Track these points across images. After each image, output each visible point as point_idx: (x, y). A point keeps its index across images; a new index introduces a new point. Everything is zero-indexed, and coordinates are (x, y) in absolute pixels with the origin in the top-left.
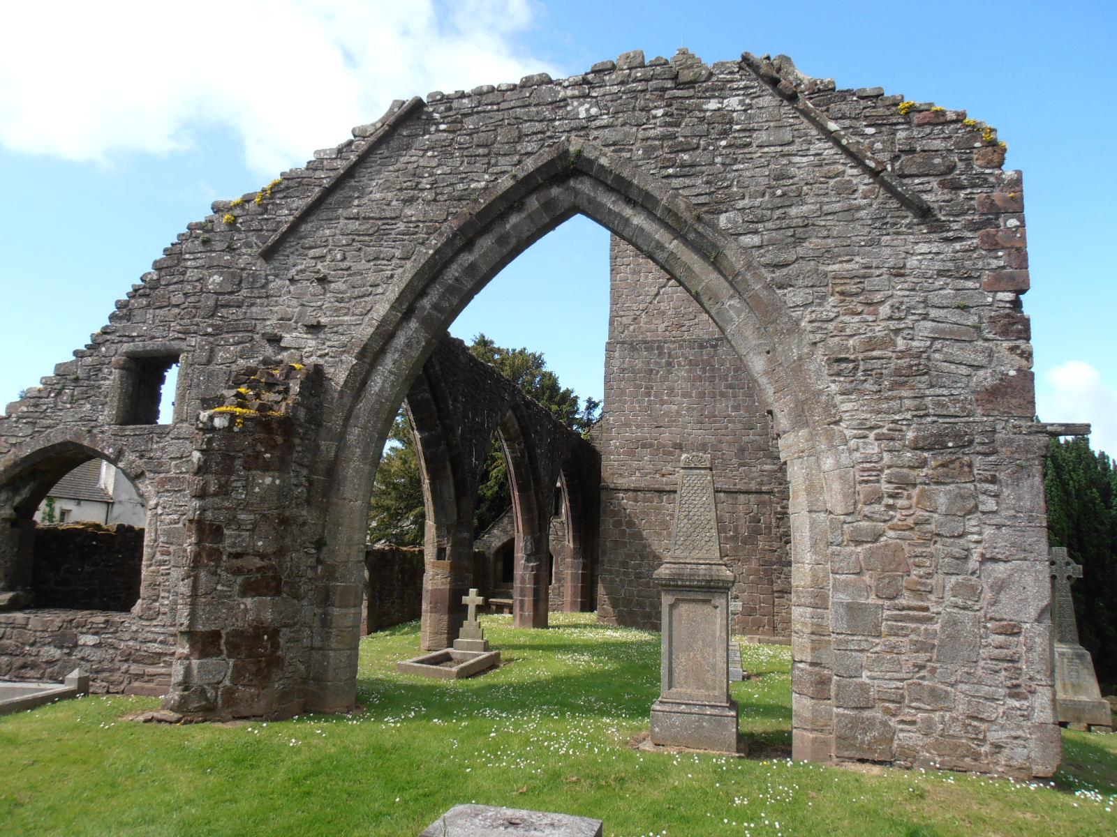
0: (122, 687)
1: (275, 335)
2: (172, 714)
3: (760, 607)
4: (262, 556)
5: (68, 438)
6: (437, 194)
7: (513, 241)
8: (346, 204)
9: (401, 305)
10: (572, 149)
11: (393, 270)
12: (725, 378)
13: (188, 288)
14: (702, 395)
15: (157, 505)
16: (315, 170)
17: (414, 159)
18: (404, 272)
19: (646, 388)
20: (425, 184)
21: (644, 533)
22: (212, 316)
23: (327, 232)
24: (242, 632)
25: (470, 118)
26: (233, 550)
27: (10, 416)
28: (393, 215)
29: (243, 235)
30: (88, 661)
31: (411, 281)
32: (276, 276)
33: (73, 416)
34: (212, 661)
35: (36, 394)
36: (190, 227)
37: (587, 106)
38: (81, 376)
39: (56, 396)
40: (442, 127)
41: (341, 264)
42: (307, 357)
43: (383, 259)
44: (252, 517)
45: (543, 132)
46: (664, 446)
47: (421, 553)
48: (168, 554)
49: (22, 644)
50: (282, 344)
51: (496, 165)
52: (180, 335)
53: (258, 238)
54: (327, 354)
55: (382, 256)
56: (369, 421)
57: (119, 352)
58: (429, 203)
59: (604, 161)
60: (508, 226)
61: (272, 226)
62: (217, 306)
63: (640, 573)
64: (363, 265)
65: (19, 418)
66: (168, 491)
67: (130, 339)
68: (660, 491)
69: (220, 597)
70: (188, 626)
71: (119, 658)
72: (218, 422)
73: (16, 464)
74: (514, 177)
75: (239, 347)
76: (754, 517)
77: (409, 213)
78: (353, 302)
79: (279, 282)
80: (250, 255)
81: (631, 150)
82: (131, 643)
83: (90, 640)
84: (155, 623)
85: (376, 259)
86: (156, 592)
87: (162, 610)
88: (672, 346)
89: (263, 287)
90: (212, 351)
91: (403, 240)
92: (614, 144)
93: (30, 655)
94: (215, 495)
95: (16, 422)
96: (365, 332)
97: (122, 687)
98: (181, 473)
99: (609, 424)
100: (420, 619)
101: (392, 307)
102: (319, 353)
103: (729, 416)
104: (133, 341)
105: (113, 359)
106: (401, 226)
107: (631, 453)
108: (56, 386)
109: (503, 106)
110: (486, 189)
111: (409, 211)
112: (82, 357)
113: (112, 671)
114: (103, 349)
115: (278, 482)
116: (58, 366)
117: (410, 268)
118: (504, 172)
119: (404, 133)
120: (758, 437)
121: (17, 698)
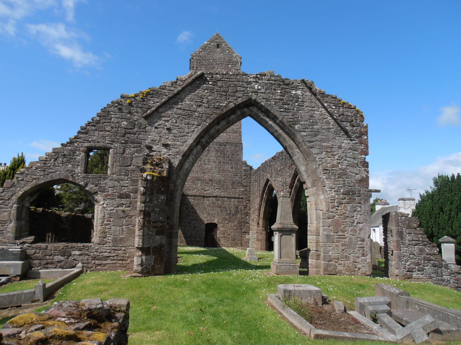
0: (92, 269)
2: (139, 274)
3: (238, 238)
4: (162, 222)
5: (62, 177)
8: (177, 104)
11: (194, 128)
13: (113, 125)
14: (220, 162)
15: (103, 204)
16: (163, 89)
17: (200, 92)
18: (198, 130)
20: (205, 101)
23: (170, 112)
28: (194, 110)
29: (135, 108)
32: (149, 125)
33: (64, 169)
34: (149, 257)
35: (45, 159)
38: (66, 154)
39: (54, 161)
40: (210, 83)
41: (175, 124)
42: (163, 155)
43: (191, 124)
44: (158, 209)
48: (110, 221)
49: (45, 255)
50: (153, 149)
51: (229, 99)
54: (171, 154)
55: (190, 123)
58: (206, 108)
59: (263, 104)
60: (230, 119)
62: (125, 133)
63: (196, 226)
66: (109, 199)
68: (204, 197)
69: (150, 236)
72: (149, 178)
73: (36, 186)
74: (235, 104)
75: (135, 149)
77: (200, 110)
78: (180, 138)
79: (150, 127)
82: (95, 253)
83: (77, 253)
84: (105, 245)
85: (188, 124)
86: (105, 235)
87: (108, 241)
89: (144, 128)
90: (124, 149)
92: (266, 99)
93: (50, 259)
94: (148, 202)
95: (35, 170)
98: (114, 193)
100: (266, 250)
101: (194, 141)
102: (168, 154)
104: (90, 143)
105: (81, 149)
106: (197, 114)
107: (193, 182)
108: (54, 157)
110: (225, 106)
111: (199, 109)
112: (66, 146)
113: (88, 263)
116: (54, 149)
117: (200, 129)
118: (232, 102)
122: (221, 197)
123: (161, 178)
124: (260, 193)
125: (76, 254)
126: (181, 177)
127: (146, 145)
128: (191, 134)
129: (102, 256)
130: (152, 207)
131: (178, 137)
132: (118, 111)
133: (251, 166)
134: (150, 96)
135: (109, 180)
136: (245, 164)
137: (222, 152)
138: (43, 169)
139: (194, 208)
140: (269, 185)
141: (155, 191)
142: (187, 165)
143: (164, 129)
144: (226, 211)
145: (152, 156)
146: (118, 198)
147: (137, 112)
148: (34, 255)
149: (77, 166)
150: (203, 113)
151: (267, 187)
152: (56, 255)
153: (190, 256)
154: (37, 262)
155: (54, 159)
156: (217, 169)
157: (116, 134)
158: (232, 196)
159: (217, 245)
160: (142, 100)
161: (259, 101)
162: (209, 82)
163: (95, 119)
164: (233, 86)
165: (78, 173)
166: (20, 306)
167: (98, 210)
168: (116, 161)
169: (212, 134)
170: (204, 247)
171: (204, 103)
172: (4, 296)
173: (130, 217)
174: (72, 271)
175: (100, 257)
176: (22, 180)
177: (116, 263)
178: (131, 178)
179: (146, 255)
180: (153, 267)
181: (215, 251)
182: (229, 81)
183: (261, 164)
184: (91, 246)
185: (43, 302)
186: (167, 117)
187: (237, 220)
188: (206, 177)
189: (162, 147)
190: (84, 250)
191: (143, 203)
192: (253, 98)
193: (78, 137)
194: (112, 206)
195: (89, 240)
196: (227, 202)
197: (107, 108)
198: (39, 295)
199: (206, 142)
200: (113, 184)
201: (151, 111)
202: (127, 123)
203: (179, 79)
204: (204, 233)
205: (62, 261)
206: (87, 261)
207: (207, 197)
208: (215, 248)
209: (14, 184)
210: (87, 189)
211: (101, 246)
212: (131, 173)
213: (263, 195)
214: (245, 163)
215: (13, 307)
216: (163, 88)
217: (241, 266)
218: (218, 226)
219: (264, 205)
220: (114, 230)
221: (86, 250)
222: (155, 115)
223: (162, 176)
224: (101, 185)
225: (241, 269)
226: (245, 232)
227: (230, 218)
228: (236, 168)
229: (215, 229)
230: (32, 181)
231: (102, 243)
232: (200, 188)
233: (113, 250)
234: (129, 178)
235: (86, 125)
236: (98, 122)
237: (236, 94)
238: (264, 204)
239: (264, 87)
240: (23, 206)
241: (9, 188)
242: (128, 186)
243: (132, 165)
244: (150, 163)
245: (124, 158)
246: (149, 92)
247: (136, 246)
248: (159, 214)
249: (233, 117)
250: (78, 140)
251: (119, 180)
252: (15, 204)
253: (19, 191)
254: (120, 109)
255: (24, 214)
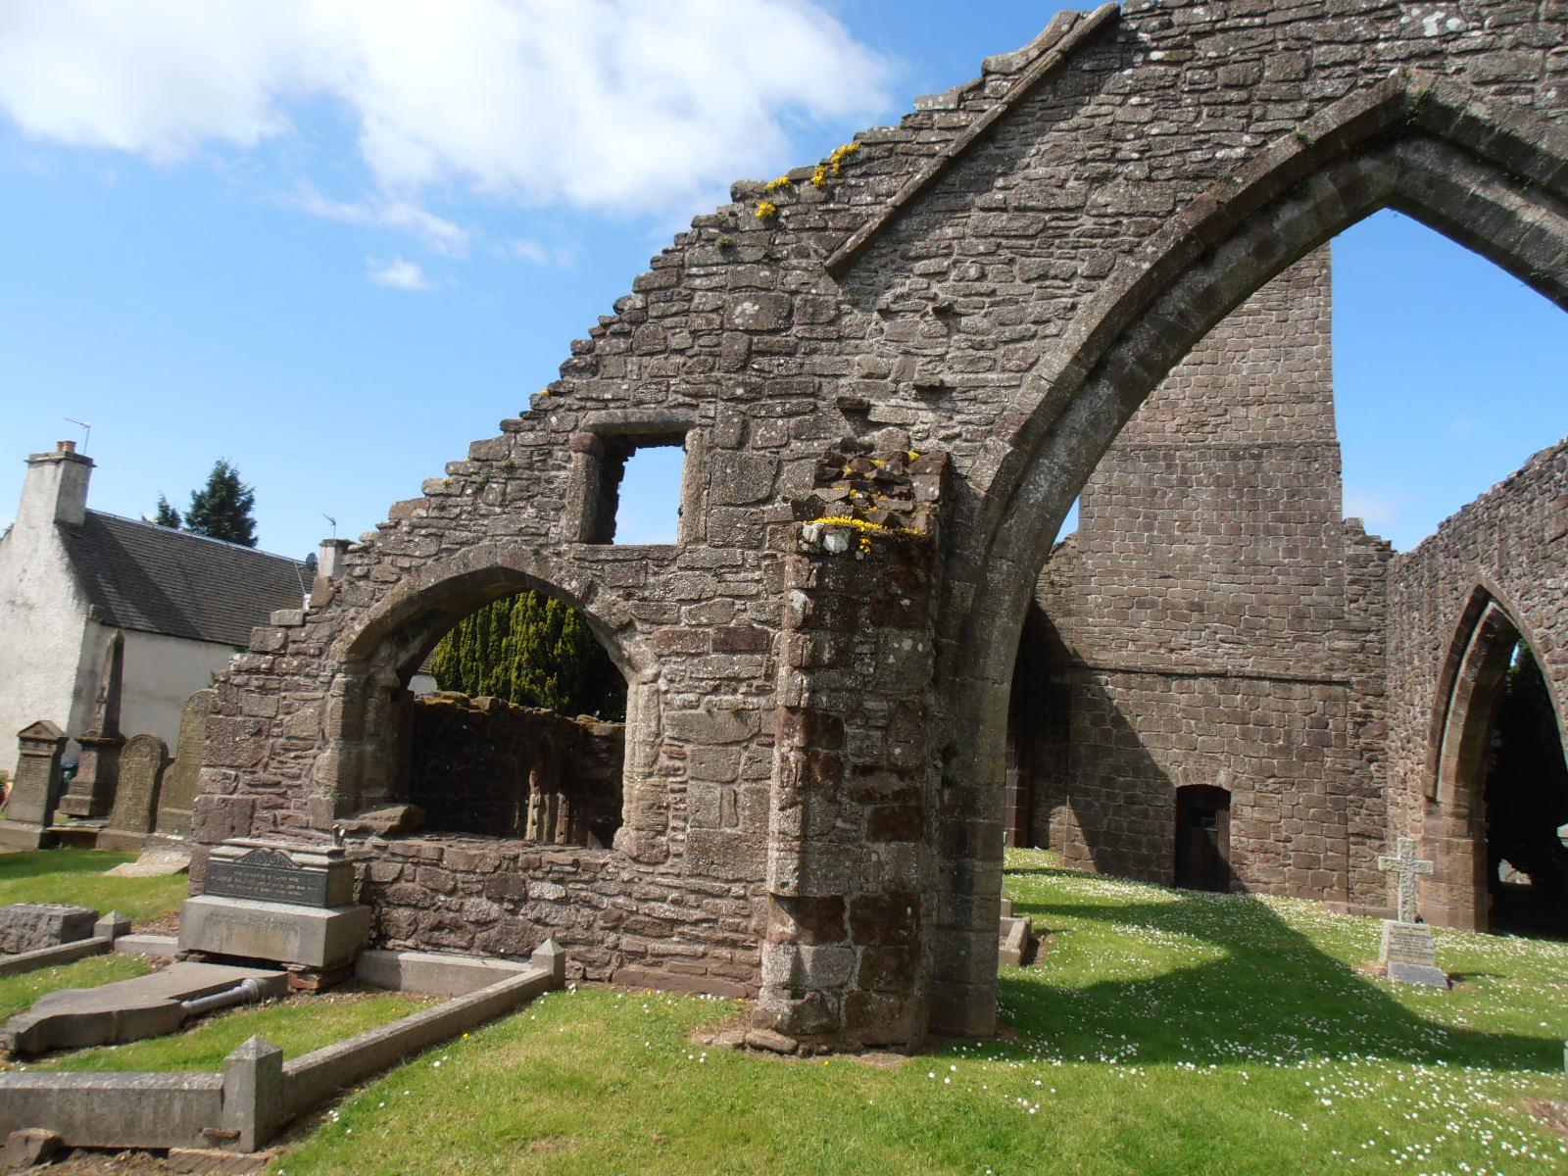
0: (608, 971)
1: (860, 402)
2: (779, 1037)
3: (1327, 858)
4: (902, 773)
5: (499, 560)
6: (1152, 169)
7: (1281, 251)
8: (984, 184)
9: (1087, 357)
10: (1413, 90)
11: (1074, 295)
12: (1272, 505)
13: (699, 322)
14: (1236, 530)
15: (657, 676)
16: (919, 129)
17: (1104, 109)
18: (1096, 300)
19: (1146, 516)
20: (1128, 150)
21: (1141, 737)
22: (743, 368)
23: (949, 232)
24: (876, 900)
25: (1210, 40)
26: (860, 761)
27: (398, 523)
28: (1071, 204)
29: (791, 237)
30: (546, 925)
31: (1109, 316)
32: (855, 304)
33: (506, 527)
34: (833, 948)
35: (441, 489)
36: (696, 224)
37: (1439, 15)
38: (516, 462)
39: (475, 493)
40: (1156, 55)
41: (977, 284)
42: (921, 440)
43: (1055, 277)
44: (884, 705)
45: (1353, 62)
46: (1174, 607)
47: (616, 742)
48: (682, 757)
49: (432, 890)
50: (872, 418)
51: (1262, 118)
52: (688, 400)
53: (819, 241)
54: (959, 435)
55: (1052, 272)
56: (1025, 550)
57: (581, 424)
58: (1137, 182)
59: (1478, 110)
60: (1277, 226)
61: (843, 221)
62: (750, 353)
63: (1134, 796)
64: (1018, 287)
65: (413, 527)
66: (678, 654)
67: (600, 405)
68: (1168, 675)
69: (842, 841)
70: (796, 889)
71: (601, 923)
72: (831, 542)
73: (410, 600)
74: (1301, 139)
75: (793, 421)
76: (1318, 719)
77: (1101, 200)
78: (1001, 350)
79: (858, 316)
80: (805, 269)
81: (1532, 91)
82: (621, 900)
83: (550, 891)
84: (662, 869)
85: (1043, 277)
86: (662, 819)
87: (673, 848)
88: (1188, 455)
89: (832, 322)
90: (745, 426)
91: (1093, 246)
92: (1497, 80)
93: (448, 909)
94: (831, 666)
95: (409, 533)
96: (1028, 398)
97: (608, 971)
98: (699, 625)
99: (1086, 570)
100: (1478, 929)
101: (1076, 359)
102: (943, 433)
103: (1278, 564)
104: (606, 407)
105: (571, 436)
106: (1087, 223)
107: (1121, 615)
108: (474, 478)
109: (1270, 19)
110: (1245, 159)
111: (1099, 197)
112: (517, 432)
113: (590, 943)
114: (554, 419)
115: (920, 647)
116: (476, 446)
117: (1106, 295)
118: (1279, 132)
119: (1086, 67)
120: (1326, 599)
121: (491, 990)
122: (1244, 677)
123: (898, 547)
124: (1436, 659)
125: (547, 896)
126: (1014, 550)
127: (841, 400)
128: (1060, 322)
129: (649, 915)
130: (850, 690)
131: (991, 346)
132: (719, 258)
133: (1384, 539)
134: (858, 172)
135: (680, 569)
136: (1357, 533)
137: (1247, 487)
138: (433, 530)
139: (1124, 719)
140: (1489, 617)
141: (864, 611)
142: (1040, 487)
143: (922, 317)
144: (1269, 737)
145: (871, 448)
146: (715, 650)
147: (802, 253)
148: (397, 886)
149: (557, 510)
150: (1122, 214)
151: (1477, 630)
152: (471, 894)
153: (1097, 930)
154: (402, 914)
155: (474, 486)
156: (1224, 558)
157: (710, 359)
158: (1296, 671)
159: (1233, 883)
160: (823, 195)
161: (1452, 100)
162: (1148, 50)
163: (629, 303)
164: (1286, 49)
165: (558, 543)
166: (162, 1153)
167: (636, 706)
168: (709, 483)
169: (1171, 319)
170: (1173, 884)
171: (1124, 161)
172: (105, 1090)
173: (766, 740)
174: (515, 973)
175: (641, 918)
176: (366, 577)
177: (704, 955)
178: (774, 556)
179: (820, 938)
180: (858, 1002)
181: (1219, 911)
182: (1263, 26)
183: (1441, 526)
184: (604, 865)
185: (255, 1151)
186: (935, 256)
187: (1324, 779)
188: (1176, 591)
189: (914, 404)
190: (578, 882)
191: (800, 668)
192: (1413, 90)
193: (562, 390)
194: (691, 689)
195: (606, 842)
196: (1270, 698)
197: (673, 251)
198: (241, 1116)
199: (1142, 360)
200: (696, 585)
201: (859, 237)
202: (757, 307)
203: (992, 68)
204: (1171, 825)
205: (490, 922)
206: (586, 934)
207: (1182, 676)
208: (1222, 898)
209: (339, 591)
210: (592, 609)
211: (643, 869)
212: (773, 533)
213: (1453, 665)
214: (1355, 530)
215: (141, 1150)
216: (916, 123)
217: (1360, 1027)
218: (1233, 799)
219: (1463, 712)
220: (700, 800)
221: (583, 882)
222: (882, 256)
223: (903, 535)
224: (647, 593)
225: (1363, 1055)
226: (1364, 836)
227: (1289, 770)
228: (1310, 554)
229: (1221, 813)
230: (399, 579)
231: (649, 857)
232: (1149, 637)
233: (692, 892)
234: (766, 557)
235: (593, 337)
236: (639, 318)
237: (1306, 88)
238: (1458, 711)
239: (1481, 20)
240: (370, 681)
241: (321, 607)
242: (758, 593)
243: (779, 498)
244: (849, 477)
245: (744, 466)
246: (855, 152)
247: (770, 886)
248: (885, 729)
249: (1289, 213)
250: (562, 400)
251: (723, 567)
252: (339, 671)
253: (353, 619)
254: (726, 248)
255: (371, 716)
